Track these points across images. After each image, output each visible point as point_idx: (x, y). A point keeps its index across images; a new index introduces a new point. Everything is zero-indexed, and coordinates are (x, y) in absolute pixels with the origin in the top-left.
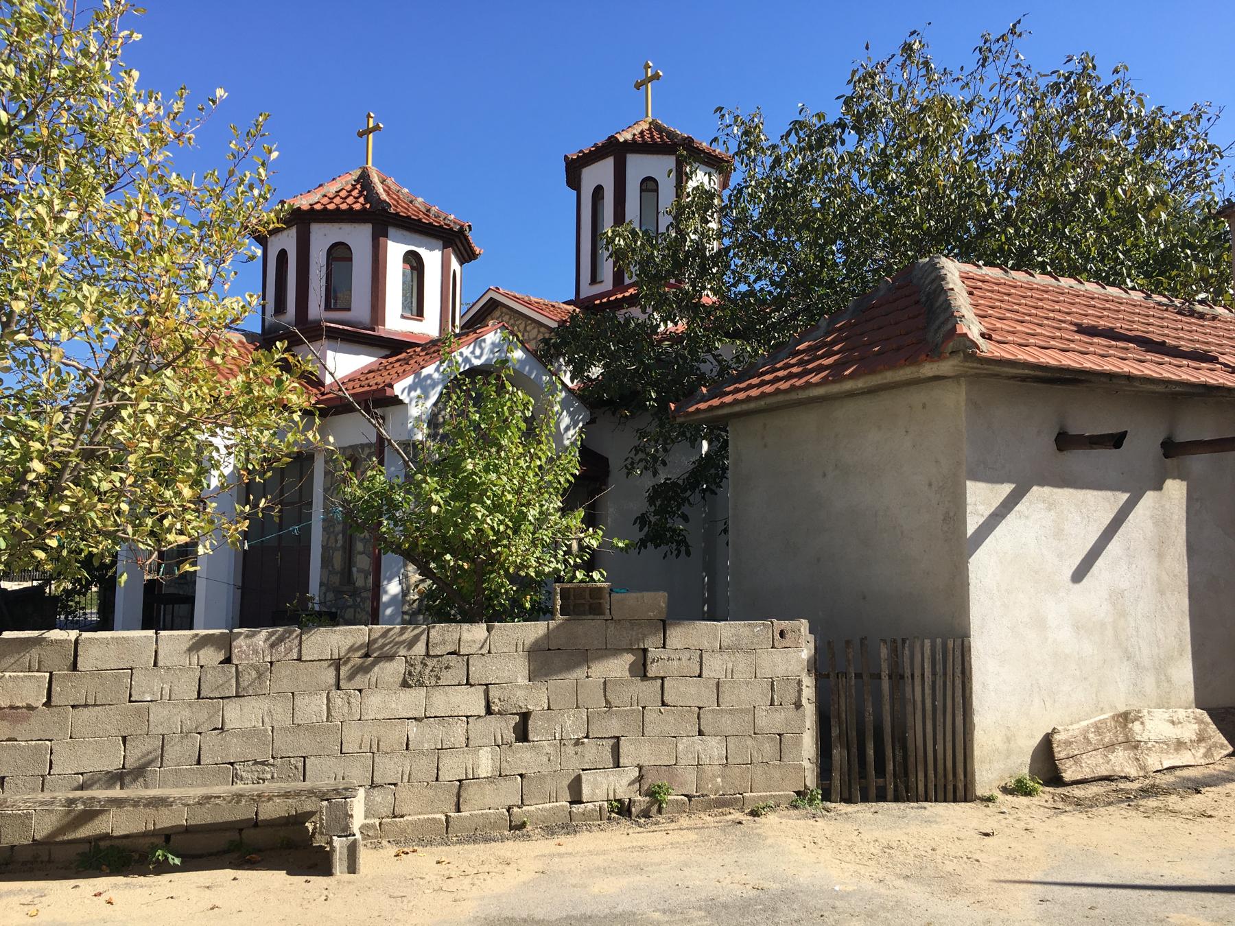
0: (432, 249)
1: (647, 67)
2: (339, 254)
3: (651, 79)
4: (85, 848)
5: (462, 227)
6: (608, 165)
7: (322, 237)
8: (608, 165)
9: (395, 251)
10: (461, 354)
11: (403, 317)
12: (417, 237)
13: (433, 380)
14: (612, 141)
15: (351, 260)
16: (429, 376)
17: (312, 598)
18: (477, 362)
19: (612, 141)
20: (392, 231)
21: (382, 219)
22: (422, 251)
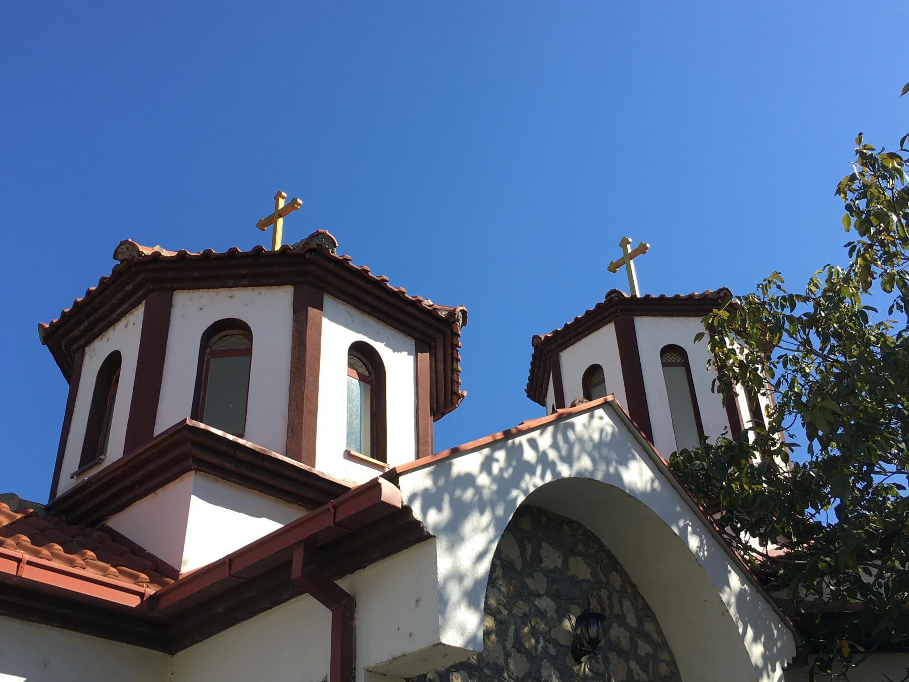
0: (396, 350)
1: (624, 243)
2: (227, 342)
3: (632, 256)
4: (499, 572)
5: (452, 314)
6: (607, 335)
7: (193, 314)
8: (607, 335)
9: (335, 337)
10: (533, 443)
11: (348, 455)
12: (371, 322)
13: (478, 490)
14: (614, 297)
15: (248, 352)
16: (468, 480)
17: (756, 639)
18: (565, 471)
19: (614, 297)
20: (329, 302)
21: (316, 275)
22: (380, 348)
